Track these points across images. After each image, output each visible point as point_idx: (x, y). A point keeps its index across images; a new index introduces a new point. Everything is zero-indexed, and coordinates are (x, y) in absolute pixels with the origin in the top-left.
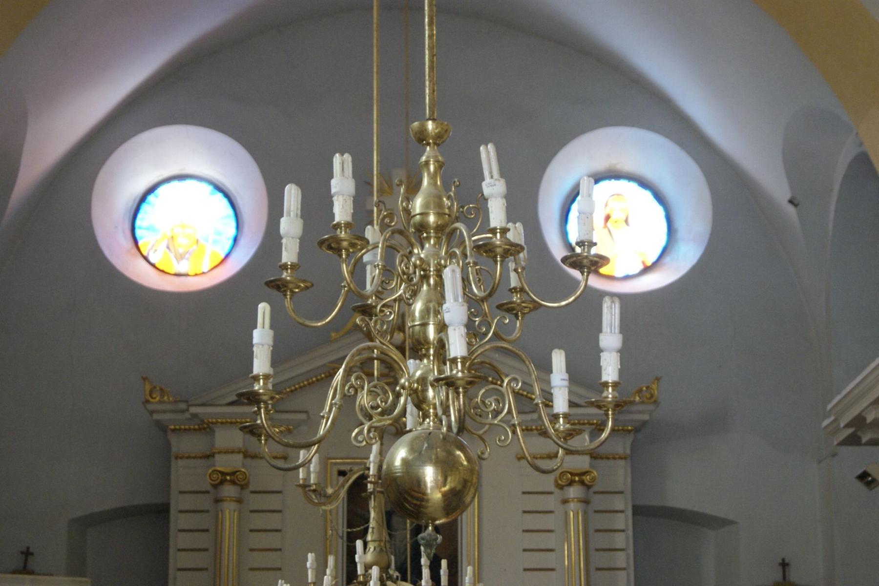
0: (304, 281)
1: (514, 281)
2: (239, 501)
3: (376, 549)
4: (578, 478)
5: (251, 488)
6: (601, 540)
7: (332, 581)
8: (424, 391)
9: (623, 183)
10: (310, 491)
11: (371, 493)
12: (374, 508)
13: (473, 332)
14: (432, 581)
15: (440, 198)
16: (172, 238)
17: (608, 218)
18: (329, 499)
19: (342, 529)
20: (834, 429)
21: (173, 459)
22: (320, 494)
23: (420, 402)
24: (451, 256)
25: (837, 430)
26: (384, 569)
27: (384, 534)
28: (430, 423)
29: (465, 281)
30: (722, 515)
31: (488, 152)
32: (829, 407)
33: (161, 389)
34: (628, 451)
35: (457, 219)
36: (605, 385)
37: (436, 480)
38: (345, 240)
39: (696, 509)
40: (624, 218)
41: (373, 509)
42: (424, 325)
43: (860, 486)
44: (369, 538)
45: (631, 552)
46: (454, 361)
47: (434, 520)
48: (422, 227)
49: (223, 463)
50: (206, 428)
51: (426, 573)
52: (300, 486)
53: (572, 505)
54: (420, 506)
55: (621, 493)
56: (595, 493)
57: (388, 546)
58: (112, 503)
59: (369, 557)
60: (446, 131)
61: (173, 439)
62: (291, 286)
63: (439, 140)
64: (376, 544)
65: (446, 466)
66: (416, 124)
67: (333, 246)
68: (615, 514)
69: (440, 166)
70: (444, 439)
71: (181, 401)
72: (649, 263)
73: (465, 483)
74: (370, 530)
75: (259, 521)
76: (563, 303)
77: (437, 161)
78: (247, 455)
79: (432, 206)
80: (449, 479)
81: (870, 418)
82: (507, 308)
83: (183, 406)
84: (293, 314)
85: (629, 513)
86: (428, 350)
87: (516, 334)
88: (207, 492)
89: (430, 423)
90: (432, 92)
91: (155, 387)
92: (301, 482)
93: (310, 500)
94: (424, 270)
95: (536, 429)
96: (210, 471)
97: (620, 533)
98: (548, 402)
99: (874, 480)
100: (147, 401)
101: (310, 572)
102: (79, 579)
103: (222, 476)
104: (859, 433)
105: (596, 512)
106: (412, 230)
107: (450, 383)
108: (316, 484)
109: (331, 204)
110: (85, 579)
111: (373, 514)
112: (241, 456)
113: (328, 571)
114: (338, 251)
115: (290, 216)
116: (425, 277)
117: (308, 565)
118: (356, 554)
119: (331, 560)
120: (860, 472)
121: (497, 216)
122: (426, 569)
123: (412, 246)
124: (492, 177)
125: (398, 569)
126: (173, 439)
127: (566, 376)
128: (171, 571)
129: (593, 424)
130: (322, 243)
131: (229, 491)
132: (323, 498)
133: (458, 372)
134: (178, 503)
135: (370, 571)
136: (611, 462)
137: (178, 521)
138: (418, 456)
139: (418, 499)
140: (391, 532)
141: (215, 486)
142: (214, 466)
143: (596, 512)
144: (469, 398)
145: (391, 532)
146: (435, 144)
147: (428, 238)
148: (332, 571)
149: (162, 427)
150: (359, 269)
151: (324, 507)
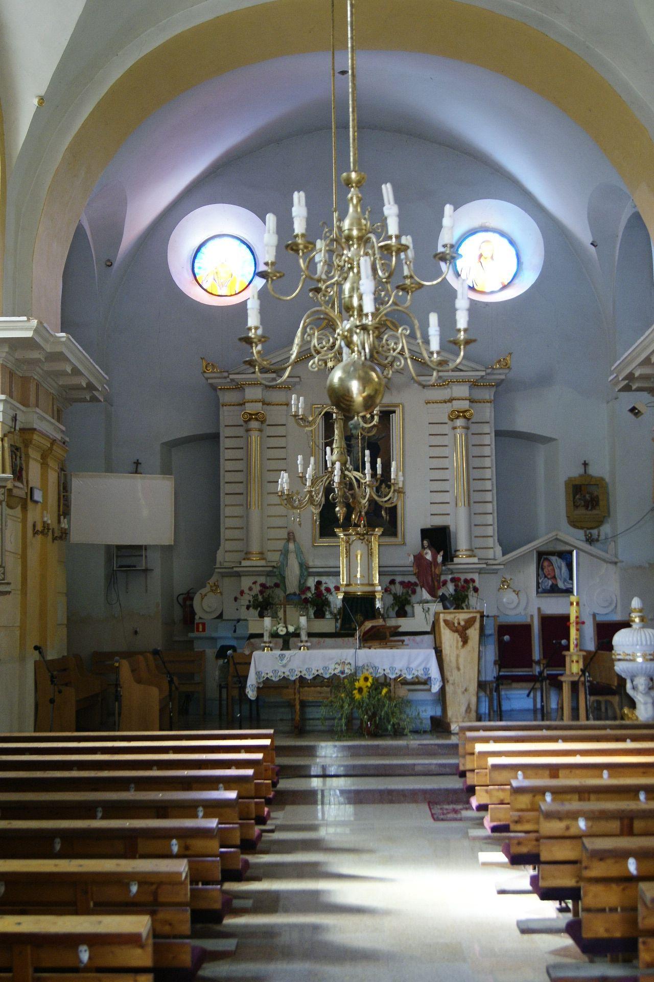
0: (278, 272)
1: (406, 272)
2: (260, 430)
4: (462, 414)
5: (268, 423)
8: (351, 336)
9: (490, 234)
13: (379, 301)
15: (359, 219)
16: (217, 273)
17: (481, 256)
18: (310, 424)
20: (615, 382)
21: (221, 406)
23: (349, 344)
24: (366, 254)
25: (618, 382)
26: (344, 464)
28: (355, 355)
29: (374, 270)
30: (549, 435)
31: (387, 189)
32: (613, 368)
33: (212, 365)
34: (492, 398)
35: (370, 232)
36: (459, 330)
37: (358, 389)
38: (301, 244)
39: (532, 432)
40: (490, 256)
42: (351, 297)
43: (630, 415)
46: (367, 315)
47: (358, 413)
48: (349, 238)
49: (250, 408)
50: (239, 387)
51: (368, 465)
53: (458, 430)
54: (350, 405)
56: (473, 423)
57: (346, 451)
58: (185, 434)
59: (335, 457)
60: (363, 178)
61: (220, 394)
62: (271, 275)
63: (359, 184)
64: (338, 450)
65: (365, 381)
66: (345, 174)
67: (294, 248)
68: (484, 435)
69: (359, 200)
70: (363, 364)
71: (224, 372)
72: (506, 284)
73: (376, 391)
74: (335, 441)
75: (273, 442)
76: (435, 282)
77: (358, 197)
78: (264, 403)
79: (355, 224)
80: (367, 389)
81: (637, 374)
82: (404, 288)
83: (226, 374)
84: (272, 293)
85: (493, 434)
86: (353, 312)
87: (408, 304)
88: (242, 426)
89: (355, 355)
90: (354, 154)
91: (209, 364)
93: (298, 424)
94: (351, 264)
95: (437, 385)
98: (427, 342)
99: (639, 411)
100: (205, 372)
101: (299, 466)
104: (631, 384)
105: (472, 434)
106: (344, 240)
107: (364, 328)
109: (292, 223)
111: (336, 432)
112: (260, 404)
113: (311, 466)
114: (297, 251)
115: (269, 232)
116: (351, 268)
117: (299, 462)
119: (312, 460)
120: (630, 407)
121: (393, 228)
123: (343, 249)
124: (389, 204)
126: (220, 394)
127: (438, 329)
129: (471, 381)
130: (287, 246)
131: (254, 424)
133: (368, 321)
134: (224, 432)
136: (482, 404)
137: (225, 443)
138: (348, 374)
139: (348, 401)
141: (246, 422)
143: (472, 434)
144: (379, 338)
146: (356, 186)
147: (353, 245)
149: (214, 388)
150: (312, 264)
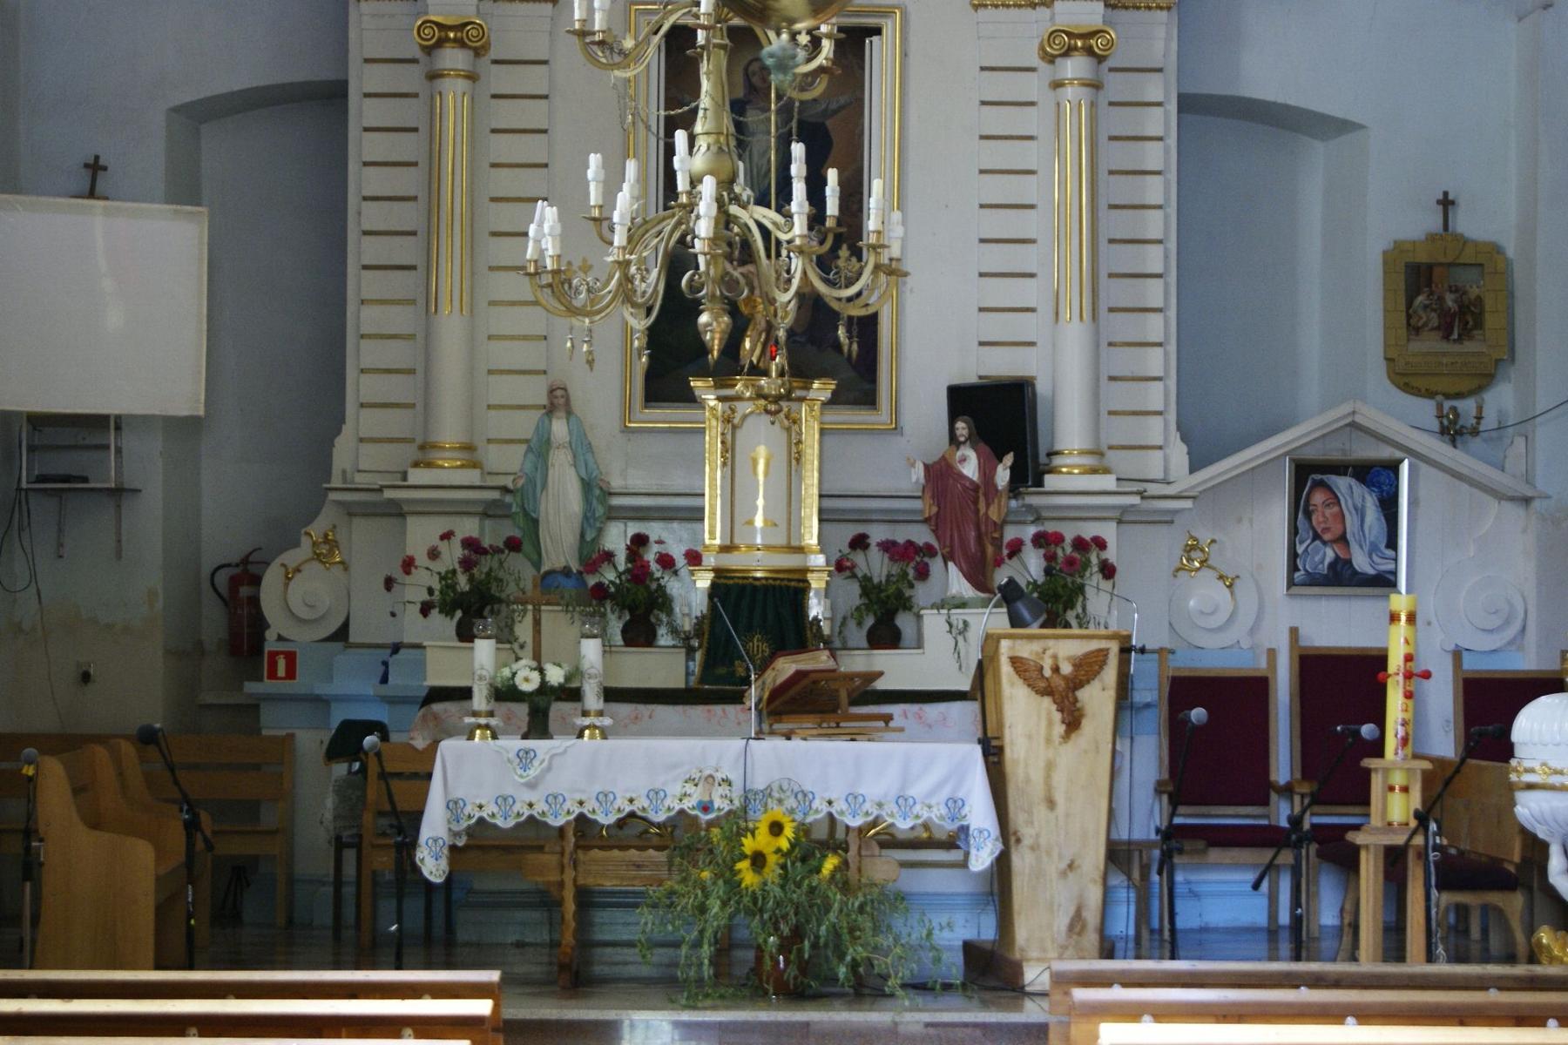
2: (472, 77)
3: (712, 148)
5: (494, 54)
6: (1121, 190)
7: (632, 205)
10: (593, 43)
11: (702, 47)
12: (707, 74)
14: (810, 204)
19: (655, 112)
22: (612, 49)
26: (726, 183)
27: (725, 120)
30: (1339, 114)
39: (1292, 102)
41: (705, 76)
44: (699, 128)
45: (1173, 176)
51: (799, 189)
52: (574, 32)
53: (1069, 92)
55: (1160, 70)
56: (1111, 70)
57: (733, 143)
59: (699, 162)
64: (711, 139)
74: (701, 113)
85: (1173, 107)
88: (414, 61)
92: (577, 26)
93: (594, 60)
96: (419, 22)
97: (1157, 383)
101: (592, 187)
102: (189, 208)
103: (440, 31)
105: (1111, 104)
108: (603, 32)
110: (200, 209)
117: (590, 174)
118: (674, 155)
119: (631, 167)
122: (799, 181)
125: (751, 182)
128: (353, 200)
131: (453, 58)
132: (615, 56)
134: (362, 80)
135: (699, 188)
137: (362, 112)
140: (742, 137)
141: (429, 50)
142: (426, 13)
143: (1111, 104)
145: (742, 137)
148: (632, 187)
151: (617, 73)
